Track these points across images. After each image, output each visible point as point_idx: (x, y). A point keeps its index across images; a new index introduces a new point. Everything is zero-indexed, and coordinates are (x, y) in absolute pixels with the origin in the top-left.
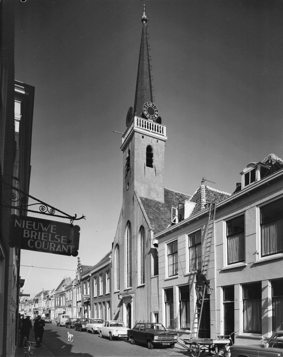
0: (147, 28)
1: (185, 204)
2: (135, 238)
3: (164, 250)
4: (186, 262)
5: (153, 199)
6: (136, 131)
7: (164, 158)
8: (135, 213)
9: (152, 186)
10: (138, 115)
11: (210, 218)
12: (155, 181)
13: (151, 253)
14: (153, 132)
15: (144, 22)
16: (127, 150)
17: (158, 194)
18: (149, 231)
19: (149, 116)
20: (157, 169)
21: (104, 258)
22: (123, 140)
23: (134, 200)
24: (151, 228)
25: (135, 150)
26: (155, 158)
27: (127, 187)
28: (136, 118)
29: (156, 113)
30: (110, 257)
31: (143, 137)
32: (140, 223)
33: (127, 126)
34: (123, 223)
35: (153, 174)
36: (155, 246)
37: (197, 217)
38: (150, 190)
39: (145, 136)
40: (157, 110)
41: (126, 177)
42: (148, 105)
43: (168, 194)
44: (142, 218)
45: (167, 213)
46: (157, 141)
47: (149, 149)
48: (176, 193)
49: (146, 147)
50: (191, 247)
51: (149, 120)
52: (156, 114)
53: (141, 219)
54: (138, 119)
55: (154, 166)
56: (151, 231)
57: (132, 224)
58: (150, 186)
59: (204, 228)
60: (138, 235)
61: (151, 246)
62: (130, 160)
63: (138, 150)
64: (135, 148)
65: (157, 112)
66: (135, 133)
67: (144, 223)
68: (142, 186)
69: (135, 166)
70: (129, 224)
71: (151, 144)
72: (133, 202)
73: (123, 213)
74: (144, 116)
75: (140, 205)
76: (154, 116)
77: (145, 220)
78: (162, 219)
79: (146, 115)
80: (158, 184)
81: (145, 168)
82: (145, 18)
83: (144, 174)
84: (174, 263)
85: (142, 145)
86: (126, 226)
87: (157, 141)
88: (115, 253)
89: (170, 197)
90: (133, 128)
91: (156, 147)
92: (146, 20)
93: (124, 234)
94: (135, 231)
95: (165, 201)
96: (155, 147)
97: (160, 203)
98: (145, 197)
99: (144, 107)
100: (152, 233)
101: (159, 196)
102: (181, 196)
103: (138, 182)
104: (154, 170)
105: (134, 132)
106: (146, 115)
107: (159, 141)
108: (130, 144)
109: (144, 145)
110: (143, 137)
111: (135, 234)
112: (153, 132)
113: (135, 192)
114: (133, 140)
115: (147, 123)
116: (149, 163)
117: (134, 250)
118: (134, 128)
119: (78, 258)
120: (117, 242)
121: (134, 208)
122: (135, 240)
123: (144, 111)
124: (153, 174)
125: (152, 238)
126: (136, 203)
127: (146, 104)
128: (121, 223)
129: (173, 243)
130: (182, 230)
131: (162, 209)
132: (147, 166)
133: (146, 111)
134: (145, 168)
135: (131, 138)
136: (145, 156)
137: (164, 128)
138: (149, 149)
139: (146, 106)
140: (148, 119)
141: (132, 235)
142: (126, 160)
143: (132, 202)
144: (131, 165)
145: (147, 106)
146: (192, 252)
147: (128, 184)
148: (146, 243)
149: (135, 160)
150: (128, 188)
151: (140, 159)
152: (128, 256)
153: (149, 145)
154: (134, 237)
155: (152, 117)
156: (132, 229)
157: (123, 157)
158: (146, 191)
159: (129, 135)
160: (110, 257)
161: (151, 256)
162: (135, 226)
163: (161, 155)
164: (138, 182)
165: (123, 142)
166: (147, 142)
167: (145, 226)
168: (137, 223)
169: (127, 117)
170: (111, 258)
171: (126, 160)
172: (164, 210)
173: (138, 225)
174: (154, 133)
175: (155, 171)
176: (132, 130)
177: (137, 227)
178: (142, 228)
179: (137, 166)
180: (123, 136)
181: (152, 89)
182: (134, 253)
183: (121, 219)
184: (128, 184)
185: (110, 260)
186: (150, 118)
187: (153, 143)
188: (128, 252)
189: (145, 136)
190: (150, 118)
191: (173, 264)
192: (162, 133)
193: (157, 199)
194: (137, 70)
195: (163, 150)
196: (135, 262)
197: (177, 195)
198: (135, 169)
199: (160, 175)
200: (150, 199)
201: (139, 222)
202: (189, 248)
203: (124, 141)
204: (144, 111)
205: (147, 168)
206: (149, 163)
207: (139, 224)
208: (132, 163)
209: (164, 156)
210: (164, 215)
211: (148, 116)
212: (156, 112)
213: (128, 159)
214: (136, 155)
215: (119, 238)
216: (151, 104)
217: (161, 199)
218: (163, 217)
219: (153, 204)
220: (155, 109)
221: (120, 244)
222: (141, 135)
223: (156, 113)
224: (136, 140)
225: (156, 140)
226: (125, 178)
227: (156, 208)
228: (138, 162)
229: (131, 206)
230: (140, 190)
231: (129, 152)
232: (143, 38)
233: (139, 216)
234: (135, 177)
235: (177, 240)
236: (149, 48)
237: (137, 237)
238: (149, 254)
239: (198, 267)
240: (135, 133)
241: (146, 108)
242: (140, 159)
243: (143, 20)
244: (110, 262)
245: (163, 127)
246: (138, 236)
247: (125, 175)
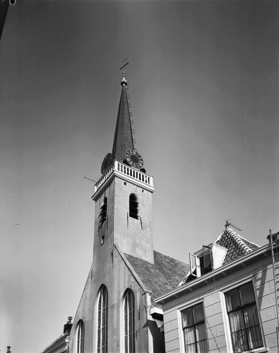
0: (127, 90)
1: (212, 248)
2: (115, 307)
3: (174, 320)
4: (224, 338)
5: (139, 257)
6: (116, 176)
7: (151, 210)
8: (115, 272)
9: (138, 241)
10: (119, 161)
11: (273, 258)
12: (140, 235)
13: (147, 326)
14: (138, 181)
15: (124, 85)
16: (102, 198)
17: (145, 252)
18: (143, 295)
19: (133, 163)
20: (143, 222)
21: (52, 346)
22: (96, 189)
23: (113, 256)
24: (145, 290)
25: (115, 196)
26: (140, 208)
27: (101, 242)
28: (116, 163)
29: (140, 161)
30: (67, 341)
31: (125, 184)
32: (124, 286)
33: (102, 173)
34: (93, 289)
35: (138, 226)
36: (153, 317)
37: (224, 272)
38: (135, 245)
39: (127, 183)
40: (142, 159)
41: (99, 228)
42: (140, 164)
43: (156, 256)
44: (129, 277)
45: (160, 276)
46: (143, 191)
47: (133, 200)
48: (165, 256)
49: (129, 195)
50: (186, 328)
51: (132, 167)
52: (140, 163)
53: (127, 280)
54: (119, 164)
55: (139, 218)
56: (148, 294)
57: (109, 289)
58: (135, 241)
59: (260, 275)
60: (121, 303)
61: (148, 317)
62: (107, 208)
63: (119, 197)
64: (116, 193)
65: (142, 161)
66: (116, 178)
67: (133, 285)
68: (124, 239)
69: (115, 214)
70: (103, 289)
71: (135, 193)
72: (112, 258)
73: (94, 275)
74: (125, 162)
75: (125, 260)
76: (139, 164)
77: (134, 280)
78: (156, 282)
79: (129, 162)
80: (145, 239)
81: (128, 218)
82: (125, 82)
83: (127, 225)
84: (198, 340)
85: (124, 191)
86: (98, 293)
87: (143, 191)
88: (75, 334)
89: (158, 258)
90: (113, 171)
91: (141, 197)
92: (126, 84)
93: (94, 304)
94: (115, 296)
95: (155, 262)
96: (140, 196)
97: (149, 263)
98: (128, 253)
99: (127, 154)
100: (149, 297)
101: (147, 254)
102: (171, 260)
103: (119, 234)
104: (140, 222)
105: (114, 176)
106: (129, 162)
107: (145, 191)
108: (107, 191)
109: (127, 193)
110: (125, 184)
111: (115, 302)
112: (138, 181)
113: (115, 245)
114: (112, 185)
115: (129, 170)
116: (134, 212)
117: (112, 327)
118: (115, 172)
119: (8, 347)
120: (81, 318)
121: (113, 267)
122: (115, 312)
123: (127, 157)
124: (138, 226)
125: (149, 303)
126: (116, 260)
127: (129, 151)
128: (88, 290)
129: (193, 307)
130: (215, 284)
131: (152, 270)
132: (130, 216)
133: (129, 158)
134: (128, 218)
135: (110, 183)
136: (128, 205)
137: (150, 178)
138: (133, 200)
139: (129, 153)
140: (131, 166)
141: (109, 304)
142: (101, 209)
143: (110, 259)
144: (108, 213)
145: (130, 154)
146: (236, 319)
147: (103, 237)
148: (136, 313)
149: (115, 207)
150: (102, 243)
151: (121, 207)
152: (99, 338)
153: (133, 193)
154: (113, 307)
155: (136, 165)
156: (109, 295)
157: (96, 207)
158: (130, 246)
159: (103, 184)
160: (67, 341)
161: (147, 332)
162: (116, 290)
163: (148, 207)
164: (119, 234)
165: (96, 190)
166: (130, 189)
167: (135, 288)
168: (119, 286)
169: (103, 164)
170: (68, 343)
171: (101, 209)
172: (155, 272)
173: (120, 289)
174: (139, 181)
175: (141, 223)
176: (111, 174)
177: (119, 292)
178: (129, 293)
179: (117, 215)
180: (96, 184)
181: (134, 141)
182: (113, 331)
183: (89, 285)
184: (103, 237)
185: (66, 345)
186: (133, 166)
187: (138, 192)
188: (99, 331)
189: (127, 183)
190: (133, 166)
191: (196, 343)
192: (148, 183)
193: (144, 258)
194: (115, 124)
195: (150, 202)
196: (115, 345)
197: (167, 258)
198: (115, 218)
199: (148, 229)
200: (136, 256)
201: (122, 286)
202: (184, 330)
203: (98, 190)
204: (127, 157)
205: (130, 218)
206: (134, 212)
207: (122, 286)
208: (110, 212)
209: (151, 208)
210: (157, 278)
211: (131, 163)
212: (140, 160)
213: (104, 208)
214: (117, 201)
215: (84, 311)
216: (135, 153)
217: (150, 259)
218: (156, 280)
219: (140, 263)
220: (139, 158)
221: (85, 320)
222: (123, 182)
223: (140, 161)
224: (116, 186)
225: (141, 189)
226: (99, 231)
227: (145, 268)
228: (119, 210)
229: (108, 265)
230: (121, 244)
231: (105, 200)
232: (123, 96)
233: (123, 276)
234: (115, 227)
235: (202, 303)
236: (129, 106)
237: (118, 307)
238: (144, 327)
239: (253, 344)
240: (116, 178)
241: (129, 155)
242: (121, 207)
243: (123, 83)
244: (66, 348)
245: (149, 178)
246: (121, 305)
247: (98, 228)
